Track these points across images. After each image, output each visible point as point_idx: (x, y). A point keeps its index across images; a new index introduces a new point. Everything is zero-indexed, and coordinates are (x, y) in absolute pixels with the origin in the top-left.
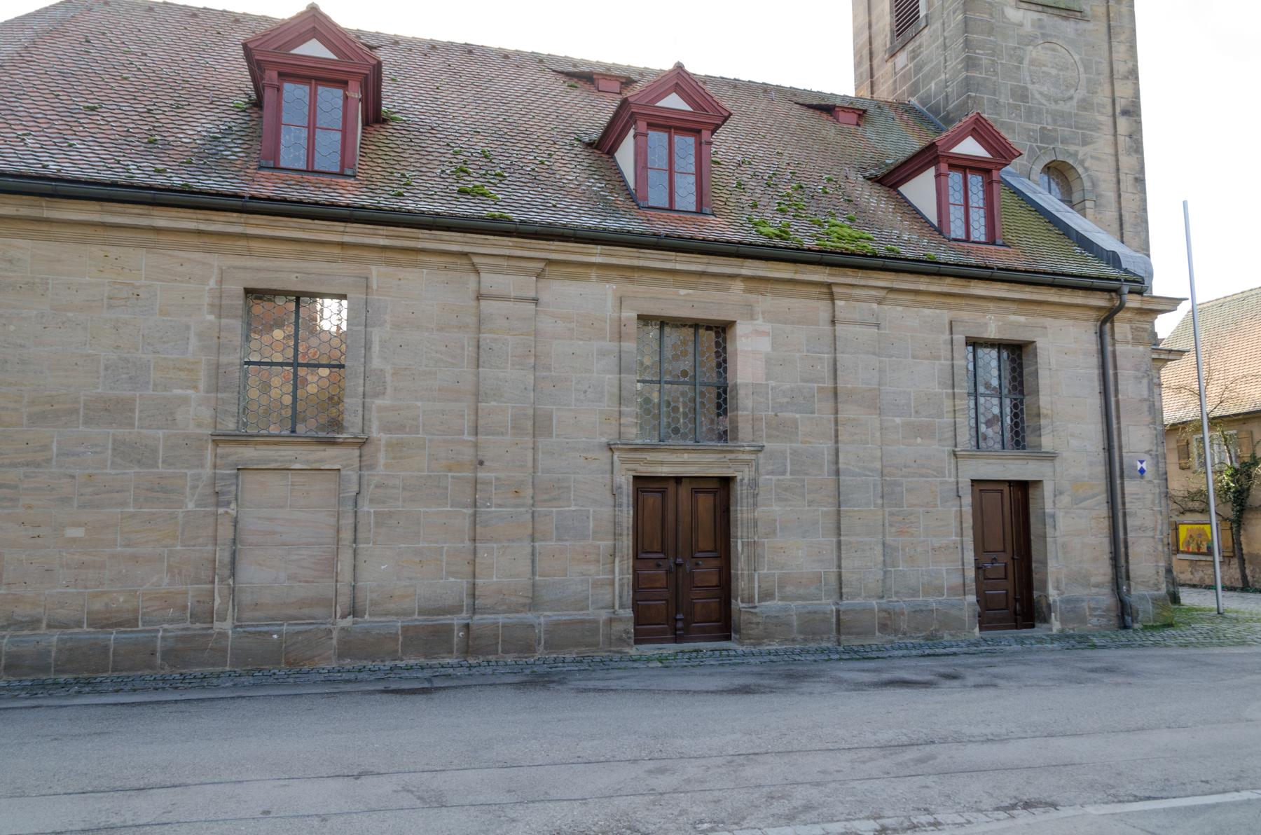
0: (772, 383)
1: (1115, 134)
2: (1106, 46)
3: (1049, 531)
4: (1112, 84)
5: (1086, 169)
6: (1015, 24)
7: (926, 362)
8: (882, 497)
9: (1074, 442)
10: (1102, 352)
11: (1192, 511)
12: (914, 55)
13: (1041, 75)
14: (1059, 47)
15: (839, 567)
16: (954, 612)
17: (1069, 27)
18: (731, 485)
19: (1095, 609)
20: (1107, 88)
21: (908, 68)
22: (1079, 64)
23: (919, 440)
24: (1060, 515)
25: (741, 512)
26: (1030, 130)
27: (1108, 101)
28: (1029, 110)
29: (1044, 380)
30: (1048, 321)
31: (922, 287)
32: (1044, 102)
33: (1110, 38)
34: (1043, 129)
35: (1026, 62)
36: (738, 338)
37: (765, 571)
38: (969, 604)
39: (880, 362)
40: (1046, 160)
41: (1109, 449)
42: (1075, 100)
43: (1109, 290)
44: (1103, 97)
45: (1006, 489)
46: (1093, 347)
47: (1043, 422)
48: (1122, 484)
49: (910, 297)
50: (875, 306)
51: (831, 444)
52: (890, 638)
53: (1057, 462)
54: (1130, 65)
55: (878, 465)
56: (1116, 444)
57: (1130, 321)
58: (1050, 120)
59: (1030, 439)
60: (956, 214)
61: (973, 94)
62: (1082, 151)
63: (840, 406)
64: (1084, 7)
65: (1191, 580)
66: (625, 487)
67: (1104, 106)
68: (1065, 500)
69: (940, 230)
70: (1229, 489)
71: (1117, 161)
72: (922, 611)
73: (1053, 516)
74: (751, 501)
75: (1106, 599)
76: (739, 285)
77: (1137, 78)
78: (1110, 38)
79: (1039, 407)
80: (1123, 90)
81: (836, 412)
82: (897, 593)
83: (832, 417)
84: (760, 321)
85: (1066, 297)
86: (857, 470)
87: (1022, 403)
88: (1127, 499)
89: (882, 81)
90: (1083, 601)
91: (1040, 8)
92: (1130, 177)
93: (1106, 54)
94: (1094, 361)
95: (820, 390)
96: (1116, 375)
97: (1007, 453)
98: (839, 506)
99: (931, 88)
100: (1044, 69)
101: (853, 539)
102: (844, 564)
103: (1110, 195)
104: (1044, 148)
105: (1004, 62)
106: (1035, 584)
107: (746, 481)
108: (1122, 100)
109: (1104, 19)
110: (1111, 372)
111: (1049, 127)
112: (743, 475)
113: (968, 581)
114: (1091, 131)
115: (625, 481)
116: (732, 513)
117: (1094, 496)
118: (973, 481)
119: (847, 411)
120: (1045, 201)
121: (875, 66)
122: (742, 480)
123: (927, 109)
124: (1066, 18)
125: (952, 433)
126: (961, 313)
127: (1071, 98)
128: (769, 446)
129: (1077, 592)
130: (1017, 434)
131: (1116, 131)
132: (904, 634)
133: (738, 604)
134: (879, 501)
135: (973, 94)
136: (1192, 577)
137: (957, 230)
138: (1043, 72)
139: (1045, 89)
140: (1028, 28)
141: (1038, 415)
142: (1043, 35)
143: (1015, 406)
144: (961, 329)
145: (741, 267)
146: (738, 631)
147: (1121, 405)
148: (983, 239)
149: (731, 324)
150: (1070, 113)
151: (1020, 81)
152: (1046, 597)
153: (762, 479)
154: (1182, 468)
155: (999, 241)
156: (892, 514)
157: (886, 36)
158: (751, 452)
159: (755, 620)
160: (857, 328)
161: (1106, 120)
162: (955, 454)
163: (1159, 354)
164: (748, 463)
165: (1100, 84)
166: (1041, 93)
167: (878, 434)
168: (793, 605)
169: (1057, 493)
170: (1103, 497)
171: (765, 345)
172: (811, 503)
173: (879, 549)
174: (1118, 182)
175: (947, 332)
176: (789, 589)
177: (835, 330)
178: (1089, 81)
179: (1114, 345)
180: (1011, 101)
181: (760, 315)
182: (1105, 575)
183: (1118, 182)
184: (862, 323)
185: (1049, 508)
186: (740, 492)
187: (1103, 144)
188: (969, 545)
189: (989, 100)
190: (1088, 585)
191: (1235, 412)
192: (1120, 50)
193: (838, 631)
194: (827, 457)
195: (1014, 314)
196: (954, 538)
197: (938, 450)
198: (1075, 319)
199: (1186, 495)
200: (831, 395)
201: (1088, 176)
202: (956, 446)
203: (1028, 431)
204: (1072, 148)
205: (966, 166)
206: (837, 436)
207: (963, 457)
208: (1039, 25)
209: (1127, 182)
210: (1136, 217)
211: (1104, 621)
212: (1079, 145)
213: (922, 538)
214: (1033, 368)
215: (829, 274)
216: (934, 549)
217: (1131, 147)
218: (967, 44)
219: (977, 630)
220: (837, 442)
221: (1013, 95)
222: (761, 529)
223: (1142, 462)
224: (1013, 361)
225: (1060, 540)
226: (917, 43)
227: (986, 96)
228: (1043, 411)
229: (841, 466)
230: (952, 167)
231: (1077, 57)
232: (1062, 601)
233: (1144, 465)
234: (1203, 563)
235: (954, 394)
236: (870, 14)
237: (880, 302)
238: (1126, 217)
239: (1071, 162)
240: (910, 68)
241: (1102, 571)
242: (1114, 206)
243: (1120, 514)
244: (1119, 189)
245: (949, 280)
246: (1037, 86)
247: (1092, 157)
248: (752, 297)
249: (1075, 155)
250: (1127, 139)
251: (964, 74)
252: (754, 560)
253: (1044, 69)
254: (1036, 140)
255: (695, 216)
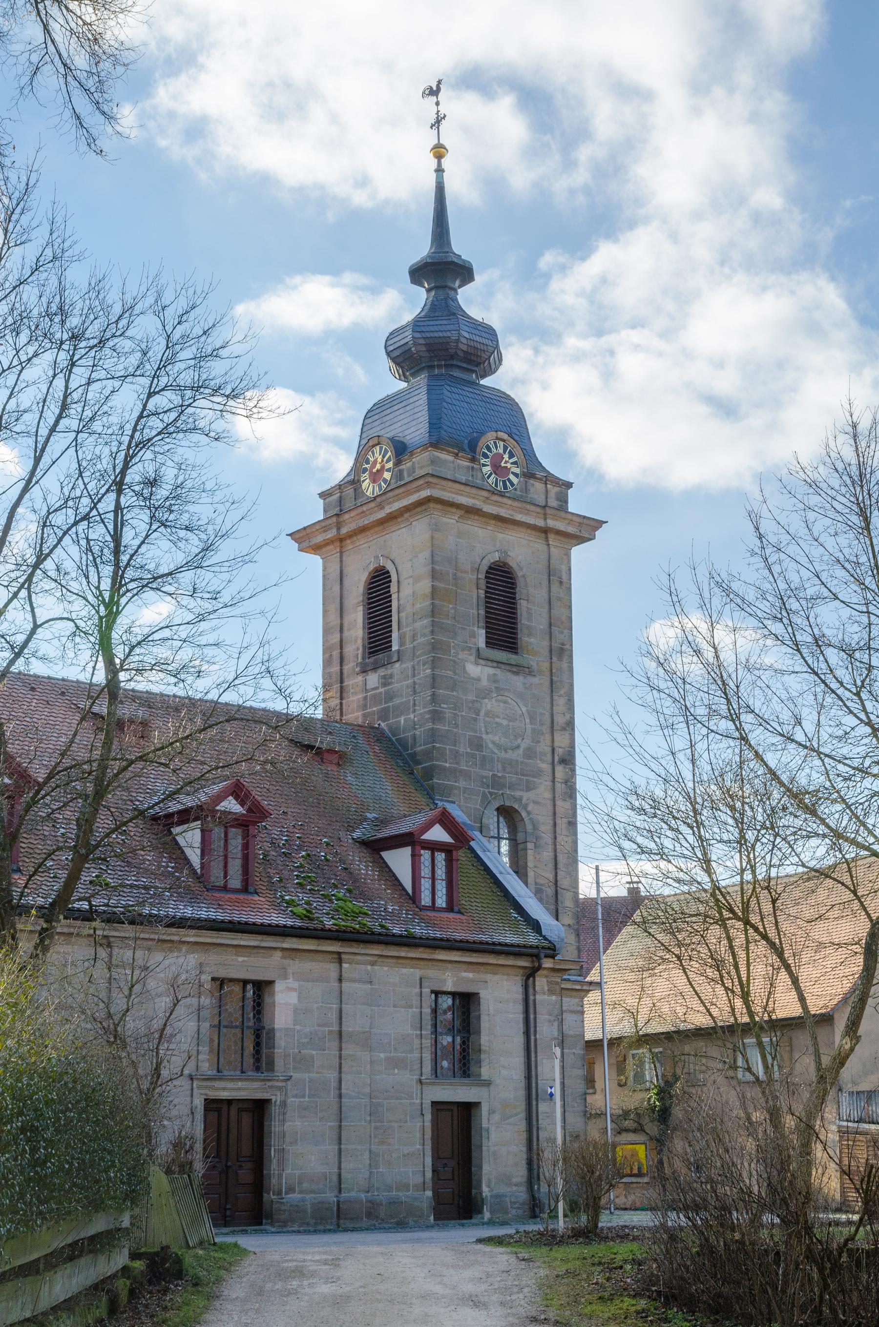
0: (298, 1027)
1: (553, 781)
2: (548, 699)
3: (484, 1141)
4: (553, 735)
5: (529, 813)
6: (473, 678)
7: (403, 1010)
8: (370, 1115)
9: (504, 1072)
10: (526, 1000)
11: (627, 1130)
12: (386, 681)
13: (494, 725)
14: (510, 700)
15: (340, 1168)
16: (416, 1204)
17: (518, 682)
18: (473, 1111)
19: (515, 1203)
20: (548, 737)
21: (378, 691)
22: (526, 715)
23: (396, 1071)
24: (492, 1129)
25: (275, 1126)
26: (483, 777)
27: (549, 749)
28: (484, 759)
29: (485, 1024)
30: (489, 977)
31: (403, 954)
32: (496, 751)
33: (552, 691)
34: (494, 776)
35: (482, 714)
36: (276, 994)
37: (290, 1171)
38: (427, 1198)
39: (372, 1010)
40: (496, 805)
41: (528, 1077)
42: (522, 750)
43: (531, 955)
44: (544, 746)
45: (455, 1108)
46: (520, 997)
47: (482, 1056)
48: (537, 1104)
49: (394, 961)
50: (369, 967)
51: (336, 1074)
52: (373, 1222)
53: (492, 1088)
54: (568, 716)
55: (368, 1090)
56: (533, 1073)
57: (546, 977)
58: (500, 767)
59: (473, 1069)
60: (426, 884)
61: (438, 745)
62: (526, 796)
63: (343, 1045)
64: (532, 663)
65: (625, 1204)
66: (199, 1107)
67: (545, 754)
68: (497, 1117)
69: (414, 898)
70: (655, 1107)
71: (554, 805)
72: (395, 1202)
73: (488, 1130)
74: (281, 1118)
75: (522, 1194)
76: (279, 954)
77: (573, 729)
78: (552, 691)
79: (480, 1045)
80: (561, 740)
81: (341, 1049)
82: (378, 1189)
83: (337, 1053)
84: (291, 980)
85: (501, 961)
86: (353, 1094)
87: (468, 1038)
88: (540, 1117)
89: (352, 691)
90: (506, 1196)
91: (495, 664)
92: (565, 820)
93: (549, 706)
94: (520, 1007)
95: (330, 1032)
96: (535, 1019)
97: (457, 1080)
98: (341, 1122)
99: (400, 722)
100: (497, 720)
101: (349, 1147)
102: (343, 1165)
103: (547, 838)
104: (495, 794)
105: (464, 714)
106: (474, 1183)
107: (278, 1103)
108: (561, 750)
109: (548, 673)
110: (532, 1016)
111: (500, 775)
112: (276, 1098)
113: (427, 1180)
114: (534, 777)
115: (199, 1102)
116: (265, 1128)
117: (516, 1115)
118: (432, 1102)
119: (349, 1049)
120: (491, 861)
121: (345, 672)
122: (275, 1102)
123: (397, 740)
124: (516, 673)
125: (419, 1065)
126: (428, 971)
127: (518, 747)
128: (296, 1075)
129: (503, 1189)
130: (464, 1065)
131: (554, 778)
132: (383, 1220)
133: (270, 1197)
134: (368, 1118)
135: (438, 745)
136: (625, 1200)
137: (426, 900)
138: (497, 723)
139: (496, 739)
140: (484, 682)
141: (480, 1050)
142: (496, 688)
143: (464, 1043)
144: (427, 984)
145: (283, 942)
146: (270, 1216)
147: (538, 1042)
148: (444, 905)
149: (270, 983)
150: (517, 761)
151: (476, 732)
152: (481, 1194)
153: (290, 1100)
154: (620, 1085)
155: (456, 909)
156: (376, 1128)
157: (358, 649)
158: (282, 1081)
159: (283, 1208)
160: (357, 985)
161: (546, 767)
162: (420, 1081)
163: (582, 986)
164: (280, 1088)
165: (543, 734)
166: (493, 743)
167: (368, 1067)
168: (308, 1197)
169: (491, 1112)
170: (523, 1115)
171: (292, 998)
172: (321, 1119)
173: (366, 1155)
174: (555, 825)
175: (418, 986)
176: (305, 1185)
177: (341, 987)
178: (533, 730)
179: (534, 995)
180: (469, 750)
181: (291, 976)
182: (522, 1176)
183: (555, 825)
184: (359, 981)
185: (485, 1124)
186: (275, 1110)
187: (543, 790)
188: (429, 1153)
189: (451, 751)
190: (510, 1185)
191: (661, 1030)
192: (560, 702)
193: (338, 1217)
194: (334, 1084)
195: (465, 971)
196: (418, 1146)
197: (408, 1078)
198: (508, 975)
199: (621, 1112)
200: (337, 1036)
201: (531, 819)
202: (421, 1075)
203: (472, 1063)
204: (518, 794)
205: (434, 847)
206: (340, 1068)
207: (427, 1083)
208: (493, 679)
209: (562, 824)
210: (568, 858)
211: (520, 1212)
212: (523, 790)
213: (396, 1147)
214: (477, 1013)
215: (341, 946)
216: (404, 1156)
217: (566, 793)
218: (434, 699)
219: (432, 1218)
220: (340, 1072)
221: (470, 745)
222: (288, 1139)
223: (551, 1088)
224: (463, 1006)
225: (492, 1149)
226: (389, 672)
227: (448, 747)
228: (483, 1048)
229: (343, 1091)
230: (424, 848)
231: (524, 709)
232: (491, 1196)
233: (553, 1090)
234: (635, 1185)
235: (421, 1035)
236: (341, 617)
237: (373, 964)
238: (560, 857)
239: (516, 807)
240: (381, 693)
241: (520, 1174)
242: (550, 848)
243: (535, 1129)
244: (555, 832)
245: (421, 949)
246: (490, 736)
247: (534, 802)
248: (286, 962)
249: (520, 800)
250: (563, 785)
251: (430, 725)
252: (282, 1162)
253: (497, 720)
254: (488, 786)
255: (241, 896)
